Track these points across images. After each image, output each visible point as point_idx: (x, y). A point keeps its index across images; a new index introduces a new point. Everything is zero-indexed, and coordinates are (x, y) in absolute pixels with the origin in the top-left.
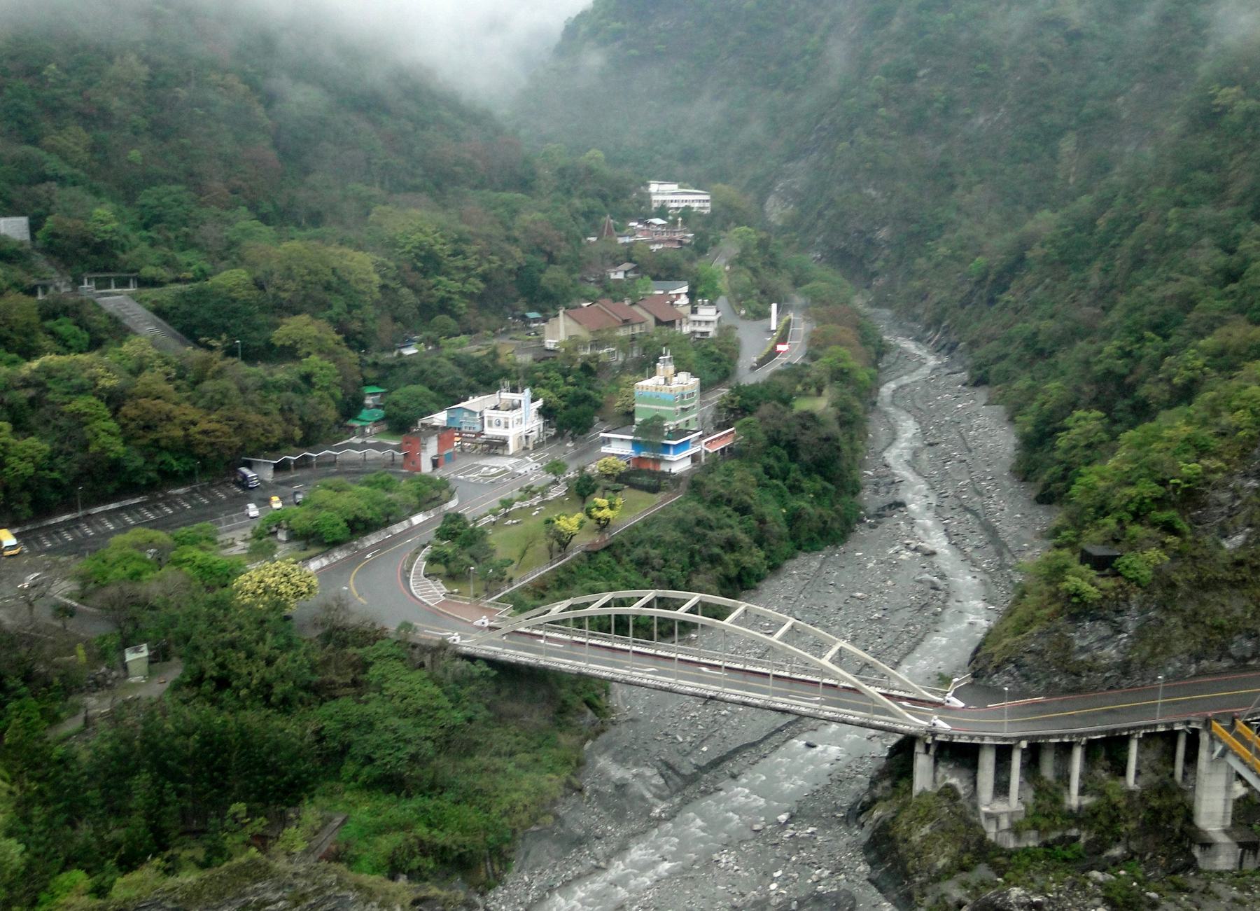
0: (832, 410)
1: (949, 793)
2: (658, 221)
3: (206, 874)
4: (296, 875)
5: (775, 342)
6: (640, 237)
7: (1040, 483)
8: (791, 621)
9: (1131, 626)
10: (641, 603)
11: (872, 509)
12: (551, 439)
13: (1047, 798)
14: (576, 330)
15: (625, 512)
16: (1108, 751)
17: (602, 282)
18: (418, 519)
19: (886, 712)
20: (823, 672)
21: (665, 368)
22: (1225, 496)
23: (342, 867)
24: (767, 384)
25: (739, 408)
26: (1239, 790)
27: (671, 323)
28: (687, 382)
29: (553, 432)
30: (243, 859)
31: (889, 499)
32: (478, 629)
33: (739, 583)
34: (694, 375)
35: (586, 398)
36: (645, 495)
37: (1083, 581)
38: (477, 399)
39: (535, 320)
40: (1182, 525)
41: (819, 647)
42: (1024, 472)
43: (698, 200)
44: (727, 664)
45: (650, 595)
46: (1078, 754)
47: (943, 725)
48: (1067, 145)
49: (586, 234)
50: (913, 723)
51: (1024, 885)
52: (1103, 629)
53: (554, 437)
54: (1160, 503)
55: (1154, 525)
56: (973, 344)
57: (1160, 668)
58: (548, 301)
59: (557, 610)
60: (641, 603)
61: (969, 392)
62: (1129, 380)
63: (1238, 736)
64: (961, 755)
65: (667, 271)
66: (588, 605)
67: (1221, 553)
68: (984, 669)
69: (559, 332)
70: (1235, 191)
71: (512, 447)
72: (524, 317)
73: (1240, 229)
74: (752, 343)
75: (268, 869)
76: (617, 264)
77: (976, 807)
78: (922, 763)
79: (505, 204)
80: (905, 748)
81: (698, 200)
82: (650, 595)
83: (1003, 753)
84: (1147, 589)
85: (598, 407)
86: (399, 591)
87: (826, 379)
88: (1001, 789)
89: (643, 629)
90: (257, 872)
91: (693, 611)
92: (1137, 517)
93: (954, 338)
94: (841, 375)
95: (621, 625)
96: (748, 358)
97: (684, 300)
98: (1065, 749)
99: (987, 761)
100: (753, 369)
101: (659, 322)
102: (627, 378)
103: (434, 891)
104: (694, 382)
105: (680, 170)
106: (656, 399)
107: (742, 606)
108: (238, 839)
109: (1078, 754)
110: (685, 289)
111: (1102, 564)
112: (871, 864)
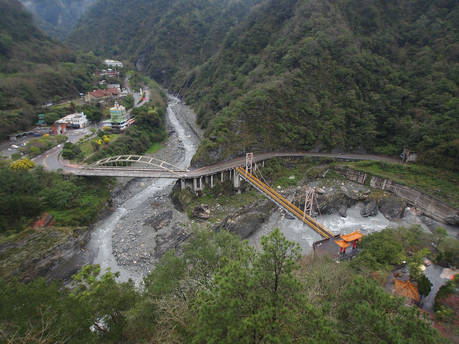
0: (156, 112)
1: (189, 189)
2: (110, 70)
3: (17, 235)
4: (42, 231)
5: (143, 97)
6: (106, 74)
7: (202, 124)
8: (152, 159)
9: (220, 152)
10: (118, 158)
11: (168, 134)
12: (91, 124)
13: (207, 186)
14: (93, 97)
15: (113, 138)
16: (218, 175)
17: (98, 85)
18: (59, 146)
19: (175, 174)
20: (160, 168)
21: (116, 105)
22: (235, 124)
23: (54, 227)
24: (142, 107)
25: (135, 113)
26: (241, 179)
27: (117, 94)
28: (122, 108)
29: (91, 122)
30: (27, 230)
31: (171, 131)
32: (75, 169)
33: (140, 152)
34: (124, 106)
35: (99, 113)
36: (117, 135)
37: (212, 144)
38: (70, 115)
39: (82, 95)
40: (228, 130)
41: (159, 163)
42: (198, 123)
43: (120, 64)
44: (377, 174)
45: (120, 157)
46: (212, 177)
47: (186, 175)
48: (201, 51)
49: (92, 73)
50: (181, 175)
51: (204, 203)
52: (215, 153)
53: (92, 123)
54: (224, 126)
55: (223, 131)
56: (186, 96)
57: (226, 159)
58: (85, 90)
59: (98, 163)
60: (118, 158)
61: (186, 107)
62: (217, 102)
63: (240, 169)
64: (190, 180)
65: (114, 82)
66: (116, 159)
67: (235, 135)
68: (194, 164)
69: (89, 98)
70: (235, 61)
71: (81, 126)
72: (79, 95)
73: (235, 69)
74: (137, 97)
75: (34, 230)
76: (101, 81)
77: (194, 190)
78: (183, 183)
79: (69, 66)
80: (179, 181)
81: (120, 64)
82: (120, 157)
83: (198, 179)
84: (223, 144)
85: (102, 115)
86: (51, 163)
87: (155, 105)
88: (198, 186)
89: (119, 164)
90: (33, 231)
91: (130, 159)
92: (220, 130)
93: (182, 95)
94: (158, 104)
95: (114, 164)
96: (136, 102)
97: (119, 89)
98: (209, 177)
99: (195, 181)
100: (140, 103)
101: (113, 94)
102: (107, 108)
103: (79, 228)
104: (124, 108)
105: (114, 57)
106: (115, 112)
107: (141, 157)
108: (25, 225)
109: (212, 177)
110: (119, 86)
111: (214, 140)
112: (174, 204)
